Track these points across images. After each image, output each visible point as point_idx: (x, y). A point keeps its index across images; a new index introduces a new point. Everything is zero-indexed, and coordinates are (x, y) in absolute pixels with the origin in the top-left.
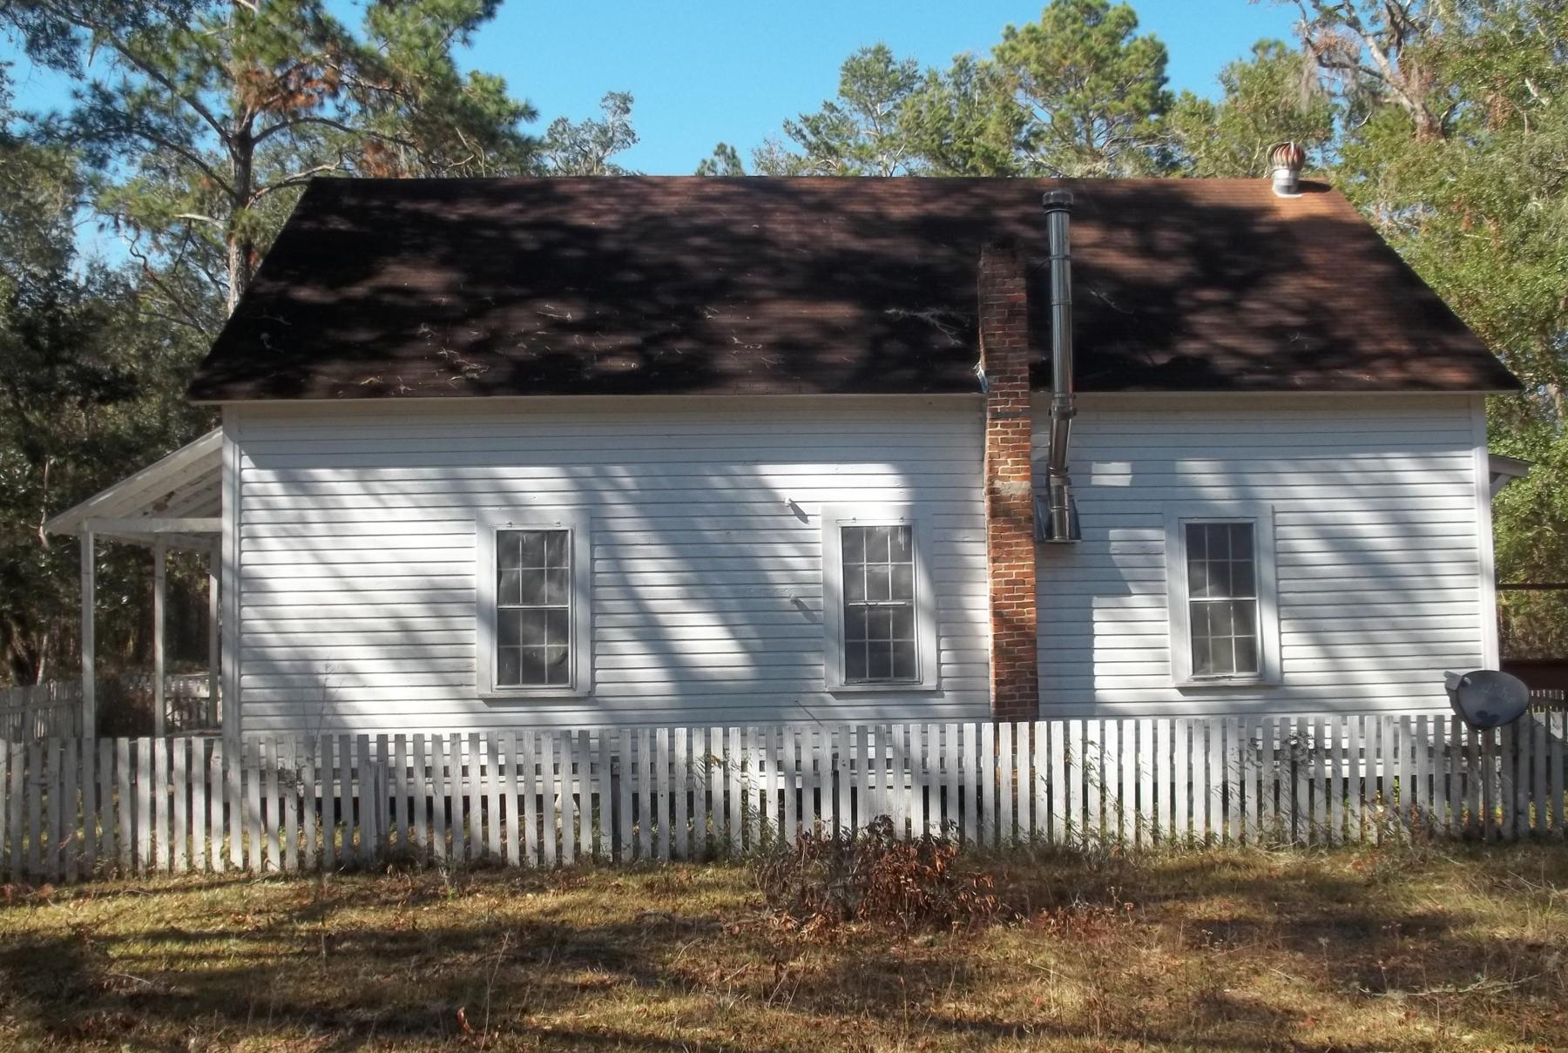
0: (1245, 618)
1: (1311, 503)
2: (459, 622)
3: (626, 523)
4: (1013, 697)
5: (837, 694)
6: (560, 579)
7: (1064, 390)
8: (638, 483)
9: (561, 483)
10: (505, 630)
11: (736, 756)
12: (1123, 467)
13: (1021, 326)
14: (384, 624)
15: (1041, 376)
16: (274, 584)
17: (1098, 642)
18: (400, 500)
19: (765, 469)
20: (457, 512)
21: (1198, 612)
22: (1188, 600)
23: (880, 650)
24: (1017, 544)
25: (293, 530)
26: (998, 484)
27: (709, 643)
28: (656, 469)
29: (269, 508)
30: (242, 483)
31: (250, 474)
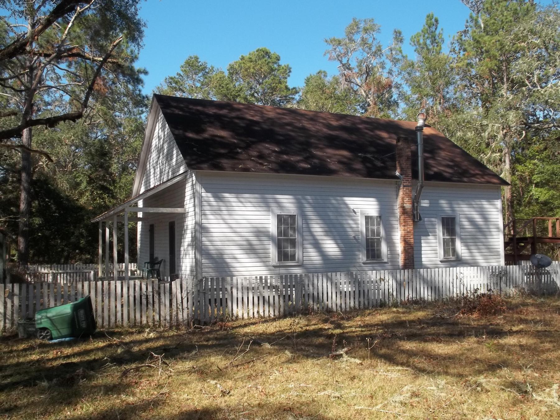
0: (453, 242)
1: (466, 212)
2: (266, 243)
3: (310, 213)
6: (294, 230)
7: (422, 180)
10: (279, 246)
11: (387, 278)
13: (409, 162)
14: (244, 243)
15: (415, 175)
16: (212, 230)
17: (423, 249)
18: (249, 204)
19: (346, 198)
20: (265, 208)
25: (217, 212)
26: (405, 205)
27: (331, 247)
28: (318, 197)
31: (204, 194)
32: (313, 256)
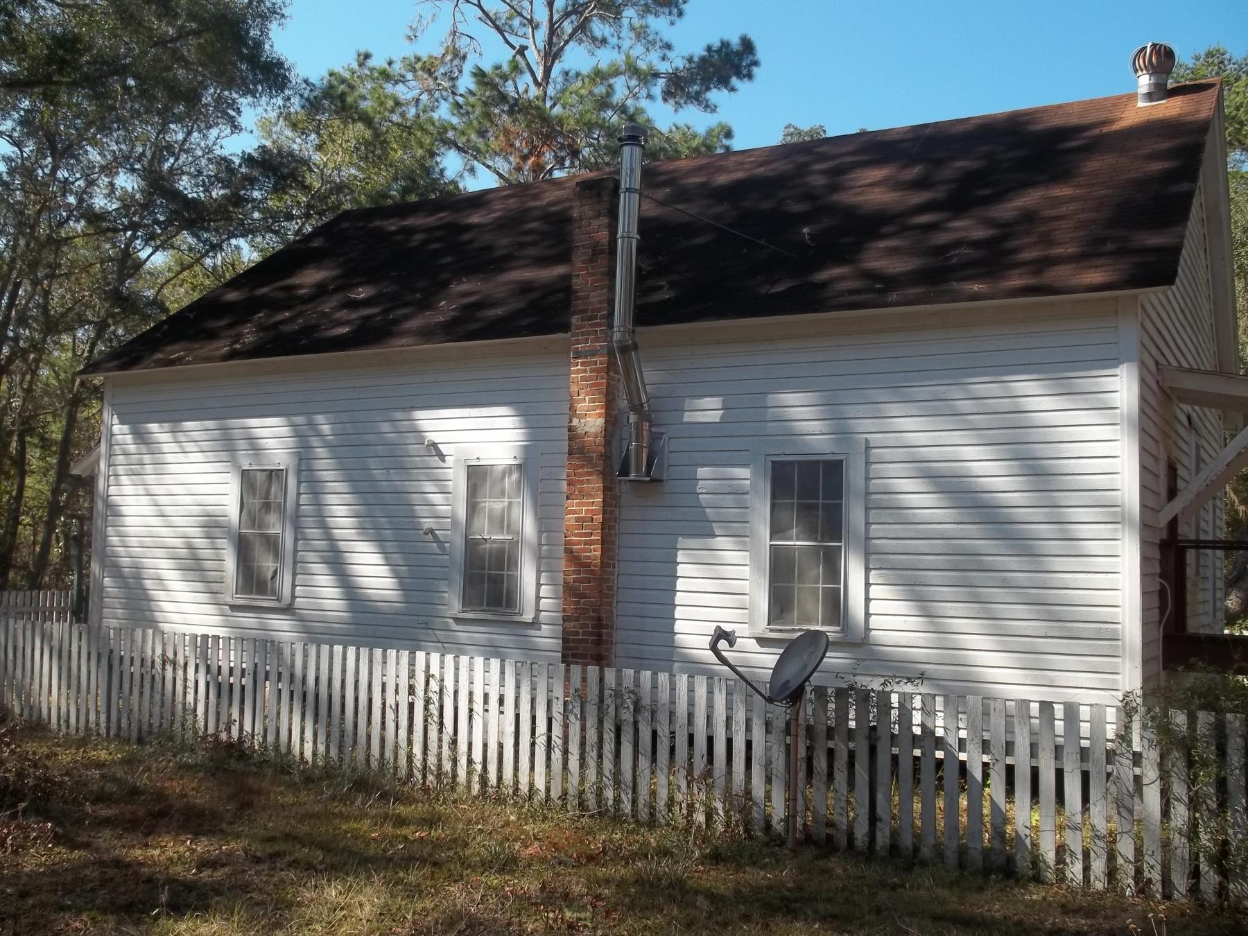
4: (577, 633)
5: (458, 620)
8: (333, 429)
9: (285, 431)
10: (243, 548)
12: (713, 402)
14: (178, 542)
16: (125, 510)
17: (680, 585)
18: (190, 447)
19: (419, 414)
21: (776, 553)
22: (768, 543)
23: (497, 581)
24: (589, 482)
26: (575, 422)
27: (373, 571)
29: (126, 454)
30: (112, 435)
32: (325, 594)
